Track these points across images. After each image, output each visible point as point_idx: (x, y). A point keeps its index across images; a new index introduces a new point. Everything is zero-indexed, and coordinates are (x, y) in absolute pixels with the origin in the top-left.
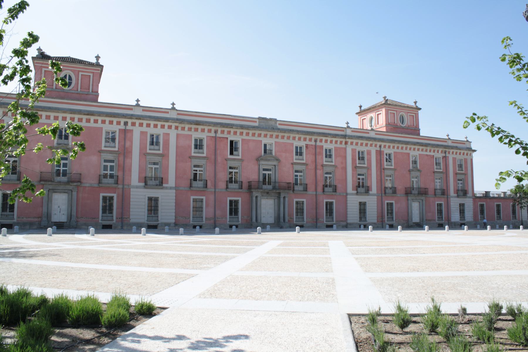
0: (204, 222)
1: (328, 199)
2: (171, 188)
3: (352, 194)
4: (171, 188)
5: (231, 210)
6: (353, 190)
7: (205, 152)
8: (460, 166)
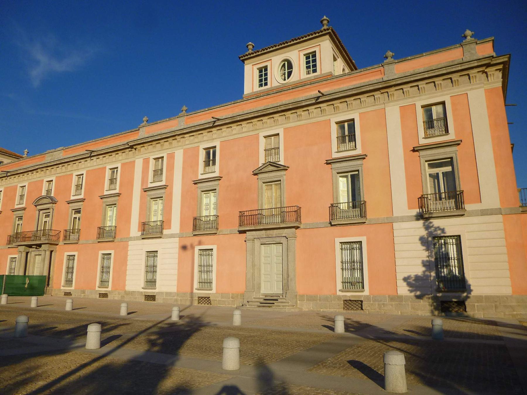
0: (110, 289)
2: (172, 236)
3: (403, 219)
4: (172, 236)
5: (68, 268)
6: (410, 208)
7: (118, 187)
8: (158, 173)
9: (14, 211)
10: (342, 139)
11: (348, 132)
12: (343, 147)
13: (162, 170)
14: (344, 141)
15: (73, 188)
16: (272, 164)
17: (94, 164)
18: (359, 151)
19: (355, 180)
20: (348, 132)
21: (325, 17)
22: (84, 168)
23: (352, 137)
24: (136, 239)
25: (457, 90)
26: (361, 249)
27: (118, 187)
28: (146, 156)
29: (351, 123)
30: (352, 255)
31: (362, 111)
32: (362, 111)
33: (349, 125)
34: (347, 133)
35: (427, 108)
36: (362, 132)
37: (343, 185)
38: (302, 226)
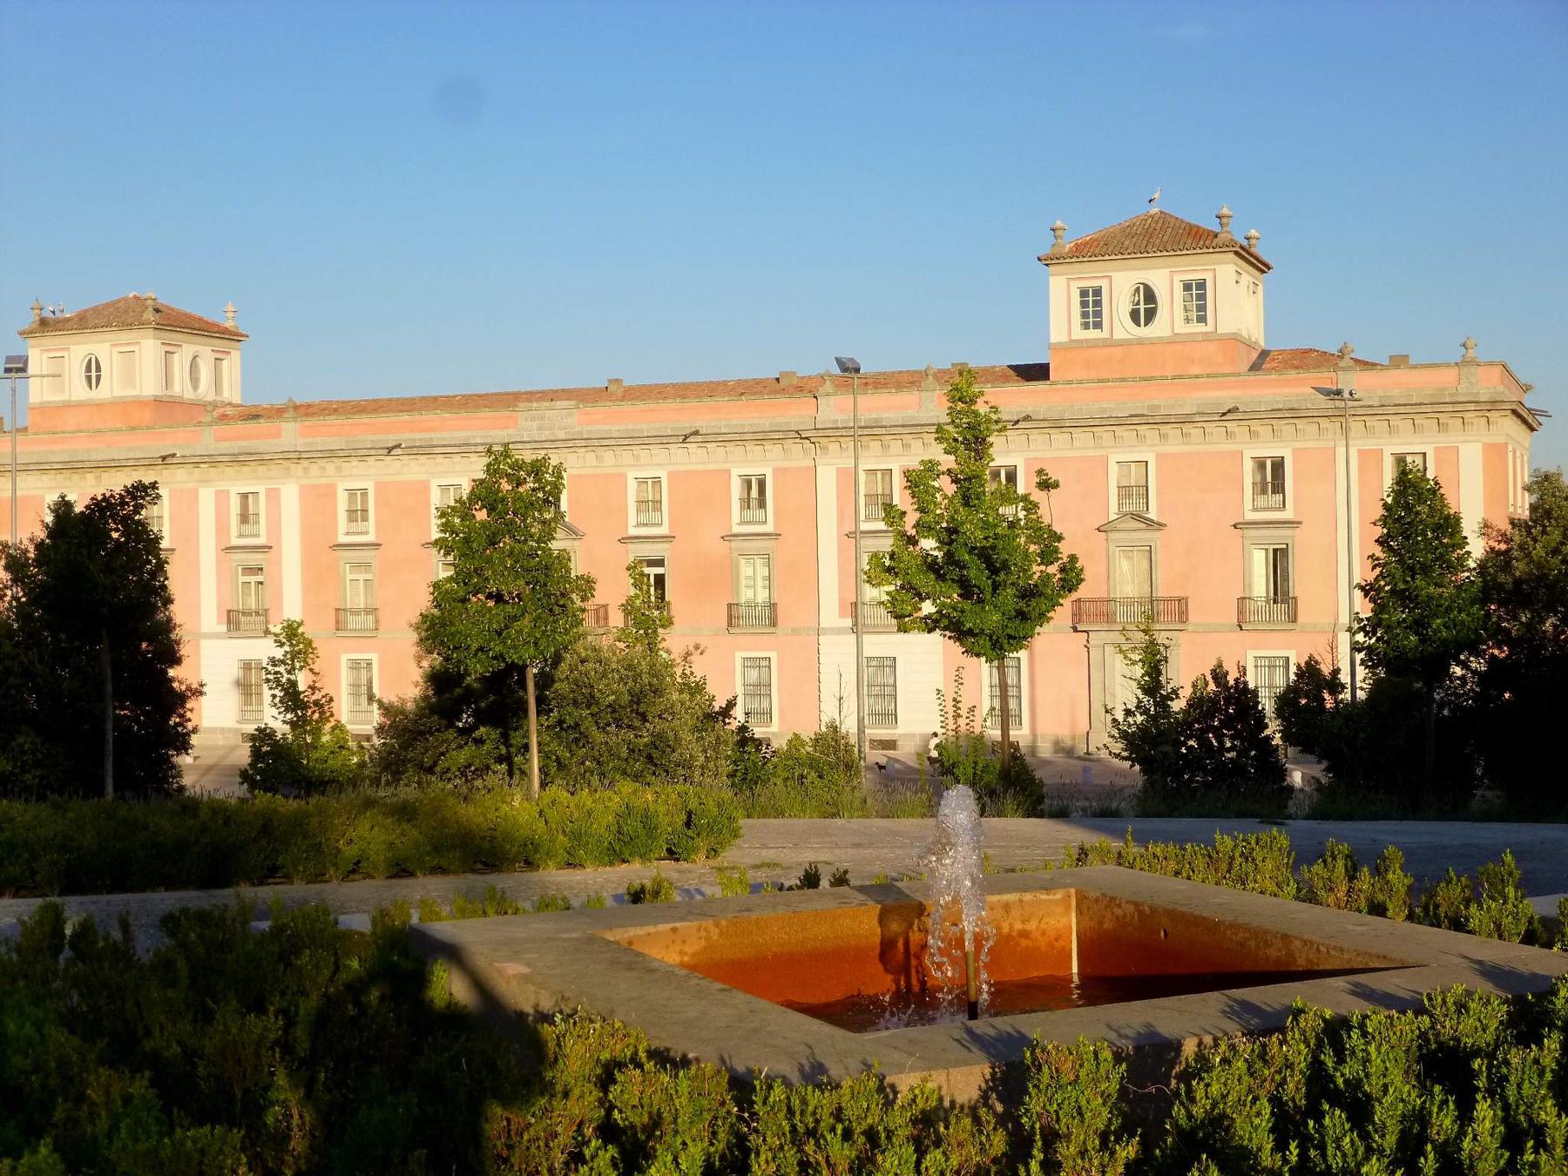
1: (355, 651)
7: (263, 531)
9: (626, 540)
10: (746, 503)
11: (1273, 477)
12: (1262, 501)
13: (365, 511)
14: (1264, 492)
15: (342, 516)
16: (1137, 517)
17: (693, 458)
18: (1288, 514)
19: (1279, 559)
20: (1273, 477)
21: (230, 308)
22: (662, 464)
23: (1278, 487)
24: (218, 636)
25: (1444, 440)
26: (1019, 668)
27: (263, 531)
28: (1370, 444)
29: (1278, 466)
30: (1271, 677)
31: (1298, 445)
32: (1298, 445)
33: (1273, 465)
34: (1269, 479)
35: (245, 496)
36: (1295, 481)
37: (1259, 563)
38: (1190, 628)
